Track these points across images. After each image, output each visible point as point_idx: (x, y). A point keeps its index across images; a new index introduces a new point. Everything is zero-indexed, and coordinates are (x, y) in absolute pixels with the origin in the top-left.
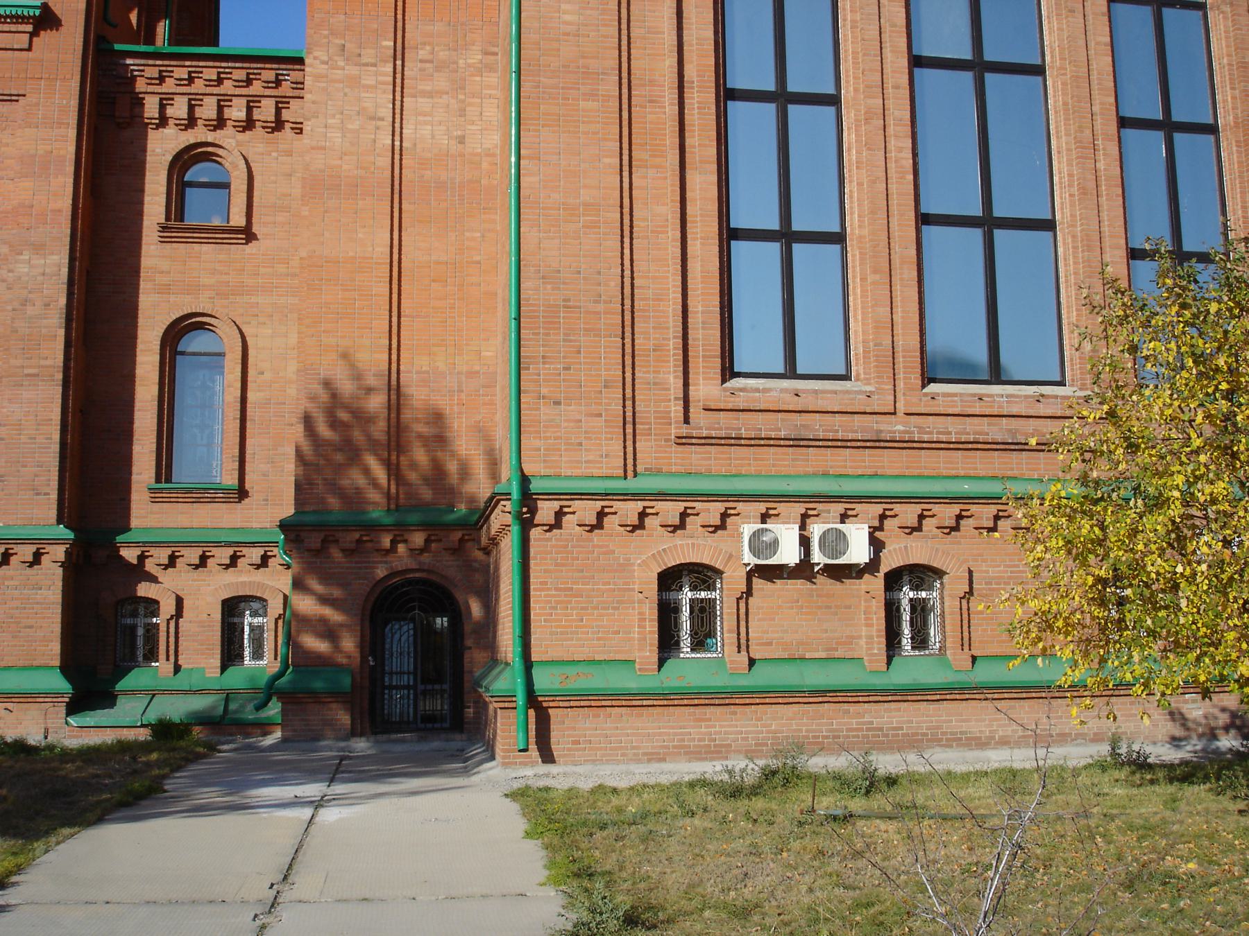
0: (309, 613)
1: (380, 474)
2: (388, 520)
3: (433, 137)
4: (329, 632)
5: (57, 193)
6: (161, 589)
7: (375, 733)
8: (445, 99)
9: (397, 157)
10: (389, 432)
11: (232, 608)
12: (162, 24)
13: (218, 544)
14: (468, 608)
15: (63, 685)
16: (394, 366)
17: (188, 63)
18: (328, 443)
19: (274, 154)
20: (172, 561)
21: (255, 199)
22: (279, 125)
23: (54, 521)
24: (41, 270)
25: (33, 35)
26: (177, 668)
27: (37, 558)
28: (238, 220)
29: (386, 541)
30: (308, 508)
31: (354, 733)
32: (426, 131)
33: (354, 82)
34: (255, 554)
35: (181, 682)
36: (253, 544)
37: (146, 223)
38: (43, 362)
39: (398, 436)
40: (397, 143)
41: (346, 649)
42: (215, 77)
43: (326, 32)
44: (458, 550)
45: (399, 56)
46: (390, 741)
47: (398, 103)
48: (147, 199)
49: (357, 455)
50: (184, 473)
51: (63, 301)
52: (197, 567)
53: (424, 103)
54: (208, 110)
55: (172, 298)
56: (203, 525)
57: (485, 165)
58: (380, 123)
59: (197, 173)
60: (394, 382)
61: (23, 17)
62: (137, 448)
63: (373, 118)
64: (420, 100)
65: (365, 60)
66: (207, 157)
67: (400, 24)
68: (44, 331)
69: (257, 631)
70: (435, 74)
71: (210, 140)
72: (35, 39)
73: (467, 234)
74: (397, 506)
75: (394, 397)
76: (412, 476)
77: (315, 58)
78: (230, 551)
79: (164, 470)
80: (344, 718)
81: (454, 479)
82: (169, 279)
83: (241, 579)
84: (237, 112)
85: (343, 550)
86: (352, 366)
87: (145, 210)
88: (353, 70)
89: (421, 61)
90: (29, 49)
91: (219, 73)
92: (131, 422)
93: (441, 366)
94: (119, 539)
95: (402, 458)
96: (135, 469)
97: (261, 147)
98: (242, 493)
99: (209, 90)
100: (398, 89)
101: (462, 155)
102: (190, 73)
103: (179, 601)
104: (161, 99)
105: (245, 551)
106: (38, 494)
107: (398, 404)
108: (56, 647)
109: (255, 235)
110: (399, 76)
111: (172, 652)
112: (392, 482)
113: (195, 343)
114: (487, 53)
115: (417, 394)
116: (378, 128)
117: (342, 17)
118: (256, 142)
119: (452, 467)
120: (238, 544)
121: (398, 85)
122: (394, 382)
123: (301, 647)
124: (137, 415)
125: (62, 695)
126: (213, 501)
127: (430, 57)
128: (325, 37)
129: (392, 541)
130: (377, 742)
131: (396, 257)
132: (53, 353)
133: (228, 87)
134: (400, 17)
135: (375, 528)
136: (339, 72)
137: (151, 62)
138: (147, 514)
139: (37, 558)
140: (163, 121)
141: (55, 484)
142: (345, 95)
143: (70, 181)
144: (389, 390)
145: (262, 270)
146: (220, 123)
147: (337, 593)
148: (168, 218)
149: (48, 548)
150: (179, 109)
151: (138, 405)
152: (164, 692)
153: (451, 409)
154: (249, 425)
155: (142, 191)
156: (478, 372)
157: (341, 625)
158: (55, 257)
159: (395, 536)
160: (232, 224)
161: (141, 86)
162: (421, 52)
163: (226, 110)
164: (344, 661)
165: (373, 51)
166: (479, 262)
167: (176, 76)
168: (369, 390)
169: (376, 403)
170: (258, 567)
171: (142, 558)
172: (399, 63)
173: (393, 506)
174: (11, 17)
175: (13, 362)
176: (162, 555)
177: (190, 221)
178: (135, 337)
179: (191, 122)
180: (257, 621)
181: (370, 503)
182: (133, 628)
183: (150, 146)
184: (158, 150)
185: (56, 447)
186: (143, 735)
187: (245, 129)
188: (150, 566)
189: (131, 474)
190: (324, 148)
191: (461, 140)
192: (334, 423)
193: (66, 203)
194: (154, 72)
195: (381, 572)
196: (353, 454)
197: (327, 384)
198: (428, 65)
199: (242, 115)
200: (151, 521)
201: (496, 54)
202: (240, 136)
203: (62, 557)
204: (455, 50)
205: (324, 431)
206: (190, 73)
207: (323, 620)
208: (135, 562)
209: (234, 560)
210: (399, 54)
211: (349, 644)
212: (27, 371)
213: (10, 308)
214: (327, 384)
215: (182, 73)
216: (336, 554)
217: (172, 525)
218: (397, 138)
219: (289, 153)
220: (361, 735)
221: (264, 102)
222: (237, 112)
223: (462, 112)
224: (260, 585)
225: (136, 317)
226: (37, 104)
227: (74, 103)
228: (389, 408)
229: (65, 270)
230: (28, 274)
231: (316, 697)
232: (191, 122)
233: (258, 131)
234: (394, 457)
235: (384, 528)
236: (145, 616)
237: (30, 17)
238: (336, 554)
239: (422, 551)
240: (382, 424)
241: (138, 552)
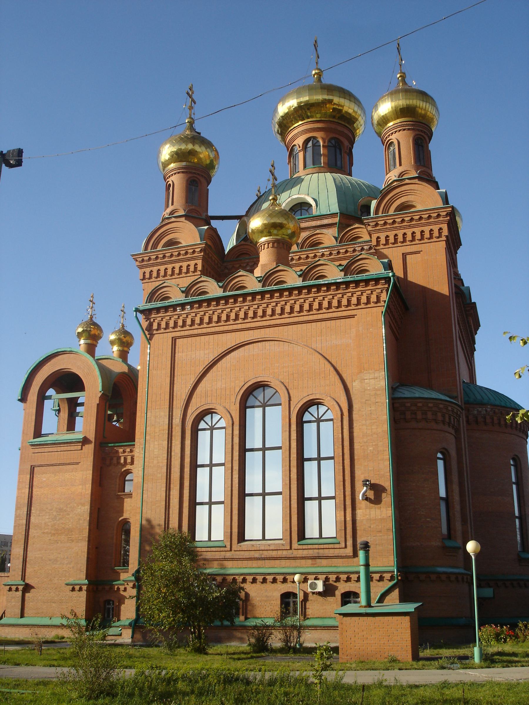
51: (88, 519)
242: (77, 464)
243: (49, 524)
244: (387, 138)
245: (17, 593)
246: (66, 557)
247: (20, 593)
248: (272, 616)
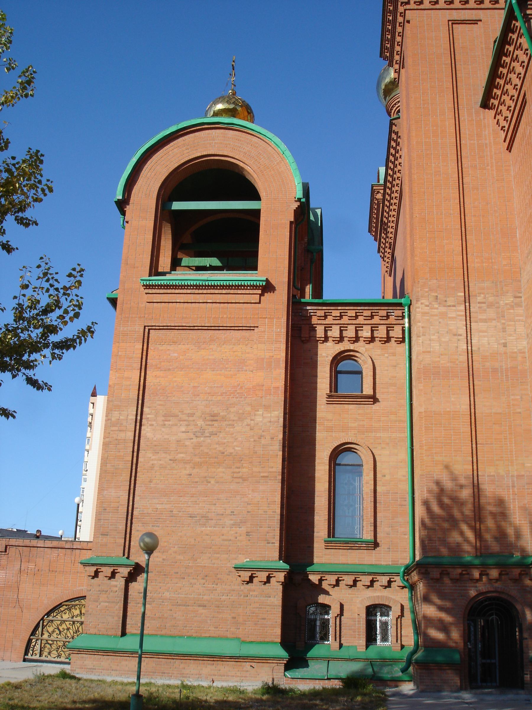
0: (433, 615)
1: (470, 535)
2: (477, 562)
3: (489, 344)
4: (443, 627)
5: (277, 378)
6: (332, 598)
7: (472, 688)
8: (494, 323)
9: (470, 355)
10: (474, 511)
11: (371, 610)
12: (308, 287)
13: (364, 573)
14: (524, 614)
15: (283, 653)
16: (475, 472)
17: (339, 308)
18: (439, 517)
19: (386, 355)
20: (338, 583)
21: (377, 380)
22: (388, 339)
23: (277, 558)
24: (269, 420)
25: (261, 295)
26: (341, 645)
27: (113, 575)
28: (368, 390)
29: (476, 574)
30: (430, 554)
31: (461, 689)
32: (485, 341)
33: (443, 315)
34: (384, 580)
35: (343, 653)
36: (383, 574)
37: (319, 393)
38: (271, 470)
39: (479, 513)
40: (469, 348)
41: (454, 638)
42: (354, 315)
43: (427, 290)
44: (517, 581)
45: (467, 301)
46: (483, 694)
47: (468, 326)
48: (319, 380)
49: (457, 524)
50: (340, 532)
51: (281, 436)
52: (351, 586)
53: (482, 326)
54: (350, 332)
55: (334, 434)
56: (353, 562)
57: (519, 358)
58: (459, 337)
59: (343, 366)
60: (476, 482)
61: (257, 286)
62: (316, 518)
63: (455, 335)
64: (480, 324)
65: (449, 303)
66: (350, 357)
67: (466, 284)
68: (271, 452)
69: (385, 625)
70: (488, 310)
71: (352, 348)
72: (262, 297)
73: (512, 397)
74: (481, 553)
75: (476, 490)
76: (488, 537)
77: (422, 304)
78: (370, 578)
79: (331, 532)
80: (457, 680)
81: (512, 538)
82: (333, 423)
83: (375, 595)
84: (366, 333)
85: (451, 579)
86: (451, 473)
87: (318, 386)
88: (443, 309)
89: (479, 303)
90: (260, 303)
91: (356, 313)
92: (314, 503)
93: (502, 472)
94: (309, 569)
95: (482, 526)
96: (316, 530)
97: (379, 352)
98: (376, 545)
99: (350, 322)
100: (468, 318)
101: (505, 353)
102: (341, 313)
103: (342, 606)
104: (325, 327)
105: (379, 578)
106: (268, 543)
107: (479, 494)
108: (278, 631)
109: (378, 399)
110: (468, 311)
111: (338, 636)
112: (477, 540)
113: (345, 459)
114: (516, 297)
115: (489, 489)
116: (459, 340)
117: (435, 281)
118: (376, 348)
119: (510, 531)
120: (323, 572)
121: (468, 316)
122: (476, 482)
123: (429, 636)
124: (317, 499)
125: (282, 659)
126: (359, 548)
127: (484, 300)
128: (427, 292)
129: (480, 574)
130: (476, 694)
131: (473, 411)
132: (276, 465)
133: (361, 320)
134: (466, 279)
135: (468, 566)
136: (435, 310)
137: (320, 308)
138: (323, 556)
139: (113, 575)
140: (326, 339)
141: (278, 538)
142: (440, 322)
143: (283, 371)
144: (474, 486)
145: (382, 419)
146: (357, 339)
147: (448, 604)
148: (331, 391)
149: (275, 574)
150: (335, 332)
151: (317, 494)
152: (334, 659)
153: (509, 497)
154: (378, 505)
155: (316, 376)
156: (523, 476)
157: (451, 624)
158: (276, 413)
159: (502, 571)
160: (364, 393)
161: (314, 320)
162: (478, 298)
163: (359, 332)
164: (454, 645)
165: (453, 299)
166: (520, 413)
167: (380, 314)
168: (461, 486)
169: (466, 494)
170: (386, 587)
171: (321, 580)
172: (467, 304)
173: (478, 554)
174: (251, 286)
175: (255, 469)
176: (332, 579)
177: (340, 393)
178: (314, 456)
179: (341, 339)
180: (384, 618)
181: (465, 552)
182: (315, 620)
183: (319, 352)
184: (324, 354)
185: (278, 517)
186: (337, 684)
187: (370, 342)
188: (325, 585)
189: (313, 532)
190: (429, 352)
191: (505, 345)
192: (441, 504)
193: (281, 384)
194: (321, 313)
195: (473, 593)
196: (454, 523)
197: (438, 483)
198: (483, 305)
199: (369, 335)
200: (324, 560)
201: (521, 297)
202: (368, 346)
203: (282, 579)
204: (497, 296)
205: (436, 509)
206: (341, 313)
207: (441, 621)
208: (317, 583)
209: (372, 584)
210: (467, 299)
211: (456, 635)
212: (262, 475)
213: (252, 440)
214: (438, 483)
215: (336, 313)
216: (447, 580)
217: (336, 562)
218: (469, 345)
219: (394, 354)
220: (466, 689)
221: (380, 327)
222: (366, 333)
223: (504, 330)
224: (387, 598)
225: (315, 445)
226: (265, 332)
227: (284, 330)
228: (474, 497)
229: (282, 420)
230: (261, 422)
231: (440, 666)
232: (341, 339)
233: (377, 343)
234: (478, 525)
235: (475, 566)
236: (321, 614)
237: (260, 286)
238: (447, 580)
239: (497, 580)
240: (470, 506)
241: (319, 577)
242: (250, 329)
243: (188, 443)
244: (395, 104)
245: (113, 582)
246: (228, 512)
247: (119, 582)
248: (375, 669)
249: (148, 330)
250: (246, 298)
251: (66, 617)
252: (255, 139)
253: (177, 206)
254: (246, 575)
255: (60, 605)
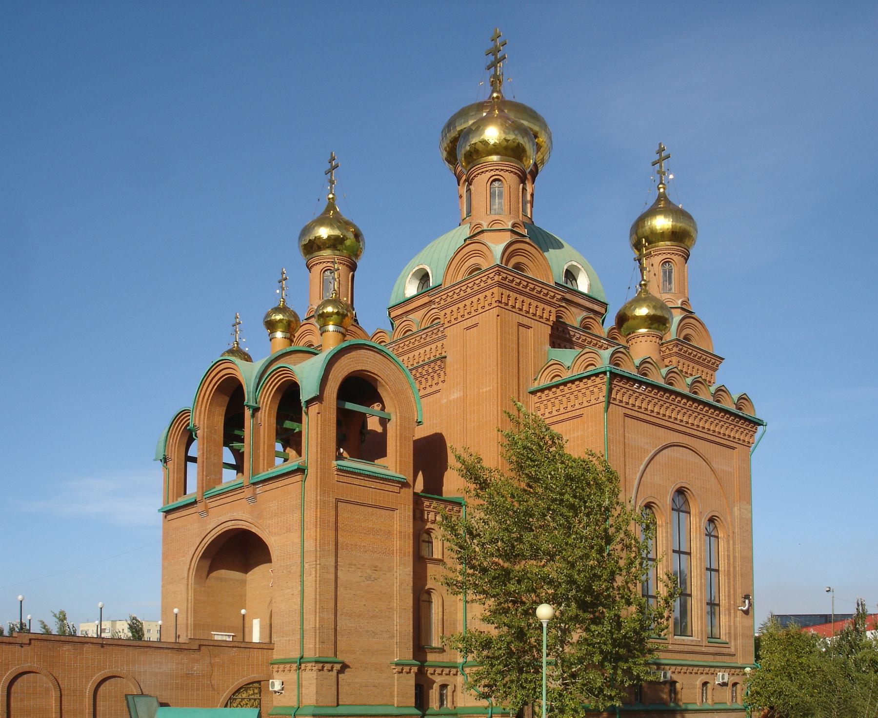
25: (401, 488)
108: (413, 700)
245: (330, 673)
249: (338, 501)
250: (391, 488)
251: (244, 696)
252: (392, 366)
253: (349, 406)
254: (399, 668)
255: (241, 688)
